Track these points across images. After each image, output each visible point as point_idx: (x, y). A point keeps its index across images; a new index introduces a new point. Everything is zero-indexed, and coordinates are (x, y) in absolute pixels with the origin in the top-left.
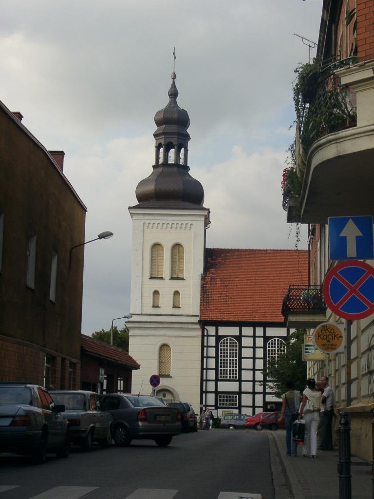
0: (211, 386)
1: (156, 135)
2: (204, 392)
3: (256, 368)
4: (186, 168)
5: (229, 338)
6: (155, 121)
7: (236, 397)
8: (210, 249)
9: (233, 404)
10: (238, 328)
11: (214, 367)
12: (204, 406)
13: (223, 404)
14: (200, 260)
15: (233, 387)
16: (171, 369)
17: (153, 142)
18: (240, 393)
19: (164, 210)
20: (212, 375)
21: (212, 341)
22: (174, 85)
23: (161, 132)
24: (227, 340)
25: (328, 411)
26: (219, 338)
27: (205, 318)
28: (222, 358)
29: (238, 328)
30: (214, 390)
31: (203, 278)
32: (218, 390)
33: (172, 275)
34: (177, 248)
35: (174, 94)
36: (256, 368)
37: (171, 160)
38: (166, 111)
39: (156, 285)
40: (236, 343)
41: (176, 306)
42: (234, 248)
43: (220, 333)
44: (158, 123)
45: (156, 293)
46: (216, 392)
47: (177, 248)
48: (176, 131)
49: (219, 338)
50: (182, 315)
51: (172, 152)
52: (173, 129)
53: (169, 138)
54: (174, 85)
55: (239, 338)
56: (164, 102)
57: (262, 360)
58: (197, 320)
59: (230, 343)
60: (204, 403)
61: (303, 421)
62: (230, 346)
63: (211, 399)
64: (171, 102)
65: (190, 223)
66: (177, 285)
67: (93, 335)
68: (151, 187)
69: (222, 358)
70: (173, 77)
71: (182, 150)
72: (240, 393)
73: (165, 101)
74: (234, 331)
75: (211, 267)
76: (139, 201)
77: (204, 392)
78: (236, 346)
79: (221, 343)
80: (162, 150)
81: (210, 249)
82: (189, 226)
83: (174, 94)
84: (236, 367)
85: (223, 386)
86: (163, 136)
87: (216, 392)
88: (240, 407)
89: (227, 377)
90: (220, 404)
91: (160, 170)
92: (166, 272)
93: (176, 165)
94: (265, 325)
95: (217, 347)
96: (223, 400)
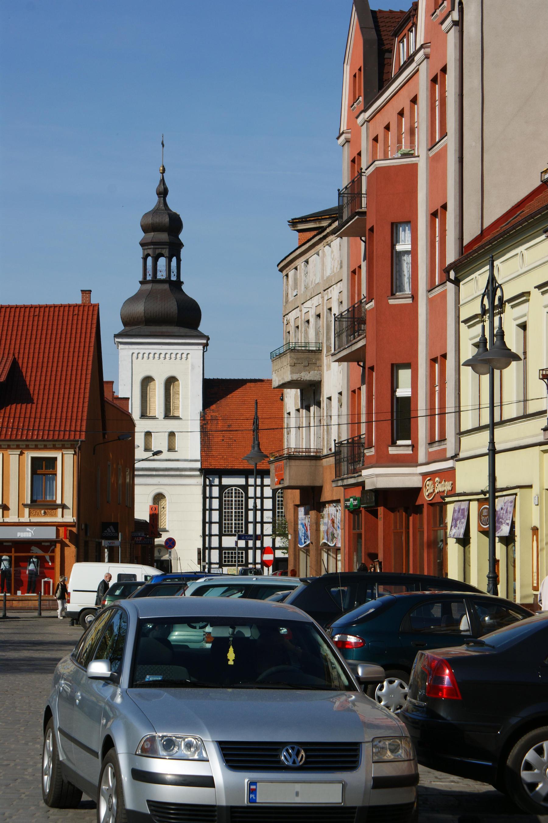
0: (215, 542)
1: (142, 244)
2: (207, 548)
3: (264, 508)
4: (178, 284)
5: (234, 488)
6: (142, 226)
8: (210, 380)
9: (228, 531)
10: (249, 512)
11: (218, 521)
12: (207, 563)
13: (229, 561)
14: (297, 794)
16: (167, 522)
17: (139, 252)
19: (155, 338)
20: (215, 529)
21: (216, 491)
22: (163, 181)
23: (149, 241)
24: (232, 490)
26: (222, 488)
27: (207, 466)
28: (227, 510)
29: (249, 487)
30: (217, 546)
31: (203, 418)
32: (223, 546)
34: (171, 382)
35: (163, 193)
36: (264, 508)
37: (162, 275)
38: (155, 212)
40: (242, 493)
43: (223, 483)
44: (146, 229)
46: (220, 548)
47: (171, 382)
48: (168, 240)
49: (222, 488)
50: (178, 460)
51: (162, 261)
52: (164, 234)
53: (158, 248)
54: (163, 181)
55: (245, 488)
56: (152, 201)
57: (271, 512)
58: (198, 465)
59: (235, 493)
60: (207, 561)
62: (235, 497)
63: (215, 556)
64: (159, 202)
65: (186, 352)
66: (171, 425)
68: (139, 308)
69: (227, 510)
70: (161, 171)
71: (174, 259)
73: (153, 201)
74: (241, 481)
75: (212, 403)
76: (125, 324)
77: (207, 548)
78: (242, 497)
80: (150, 260)
81: (210, 379)
82: (184, 356)
83: (163, 193)
84: (242, 509)
85: (229, 542)
86: (152, 247)
87: (220, 548)
89: (232, 531)
90: (225, 561)
91: (149, 287)
93: (167, 280)
95: (220, 498)
96: (229, 557)
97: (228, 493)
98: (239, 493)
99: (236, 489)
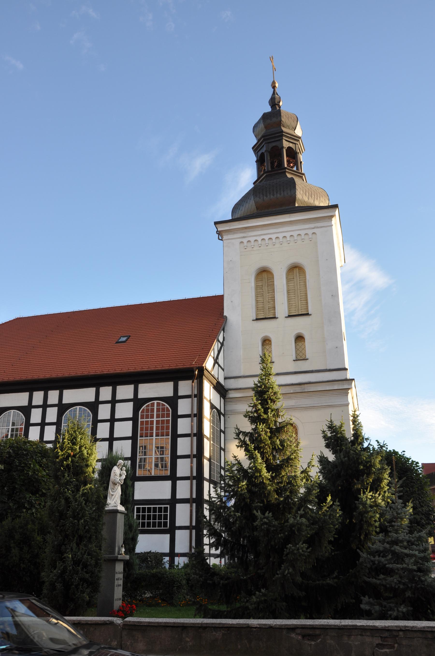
5: (155, 402)
7: (166, 509)
15: (160, 490)
18: (174, 501)
24: (153, 405)
25: (283, 502)
26: (138, 403)
33: (257, 314)
35: (274, 102)
39: (266, 328)
41: (300, 357)
42: (13, 319)
43: (141, 395)
45: (299, 338)
49: (62, 408)
55: (173, 401)
59: (158, 410)
61: (361, 553)
66: (299, 325)
67: (333, 454)
72: (174, 501)
79: (143, 411)
83: (274, 102)
85: (143, 491)
88: (172, 530)
92: (282, 307)
94: (136, 378)
97: (147, 411)
98: (163, 410)
99: (158, 404)
